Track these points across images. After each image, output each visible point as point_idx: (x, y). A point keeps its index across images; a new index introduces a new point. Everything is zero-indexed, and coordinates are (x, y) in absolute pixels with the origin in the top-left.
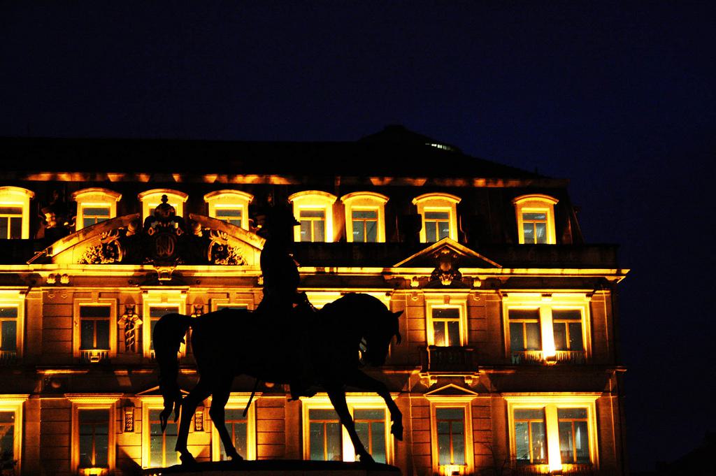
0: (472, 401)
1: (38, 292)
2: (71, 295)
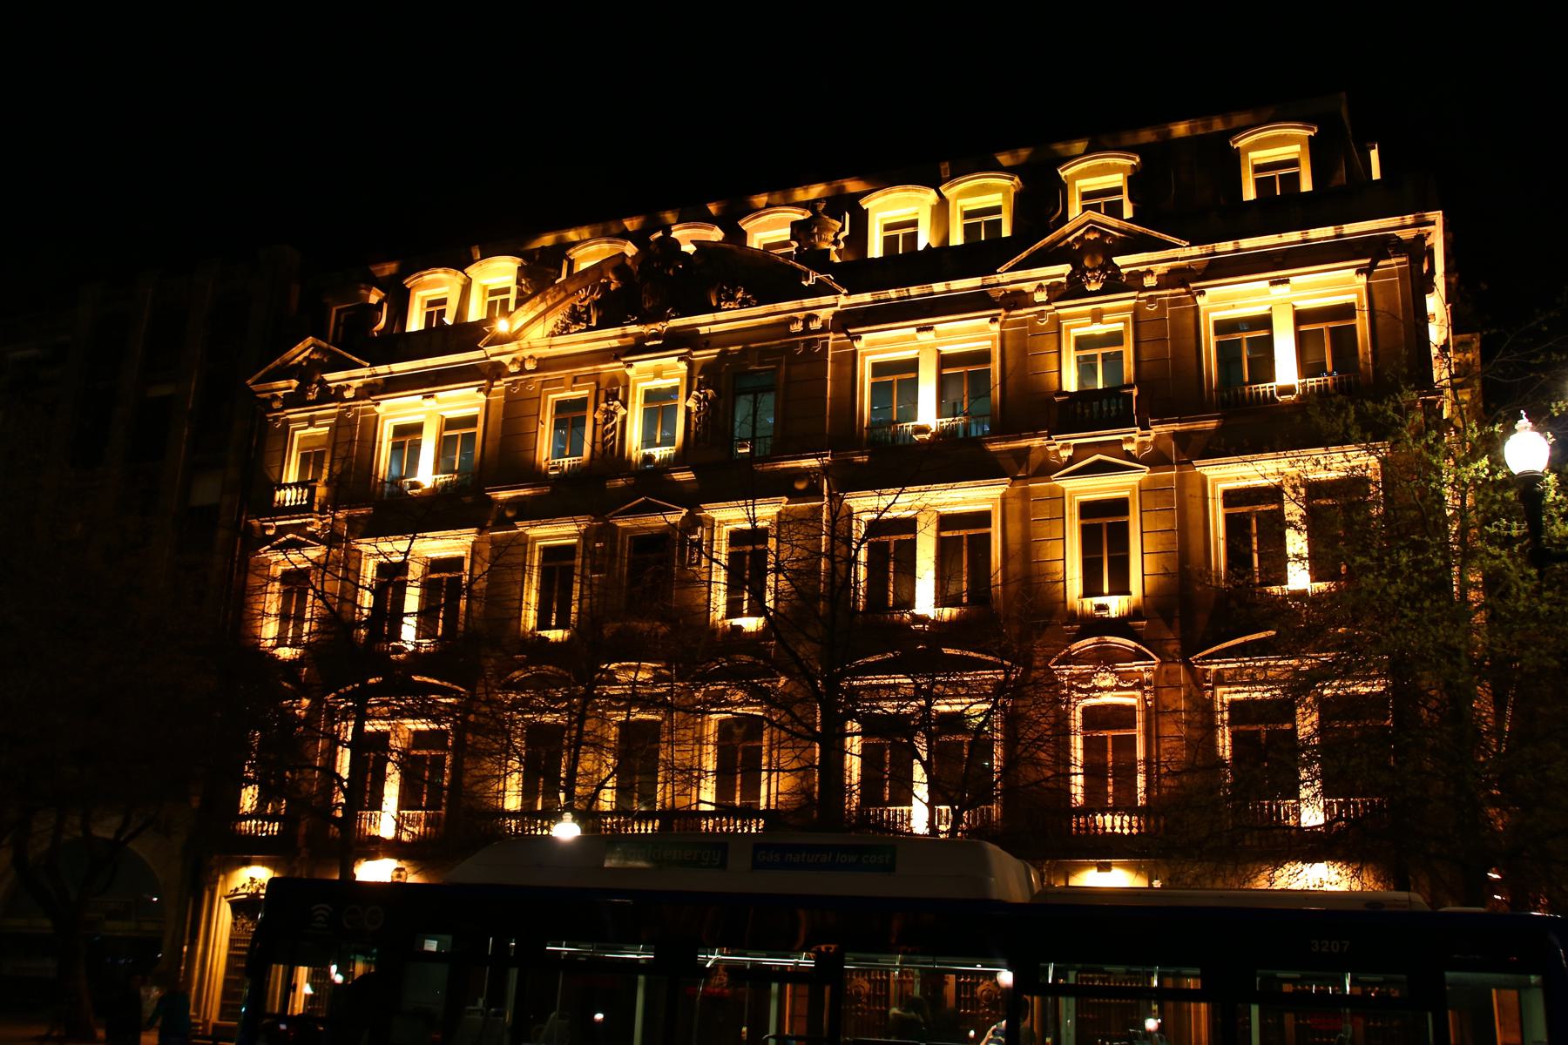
1: (500, 385)
2: (539, 384)
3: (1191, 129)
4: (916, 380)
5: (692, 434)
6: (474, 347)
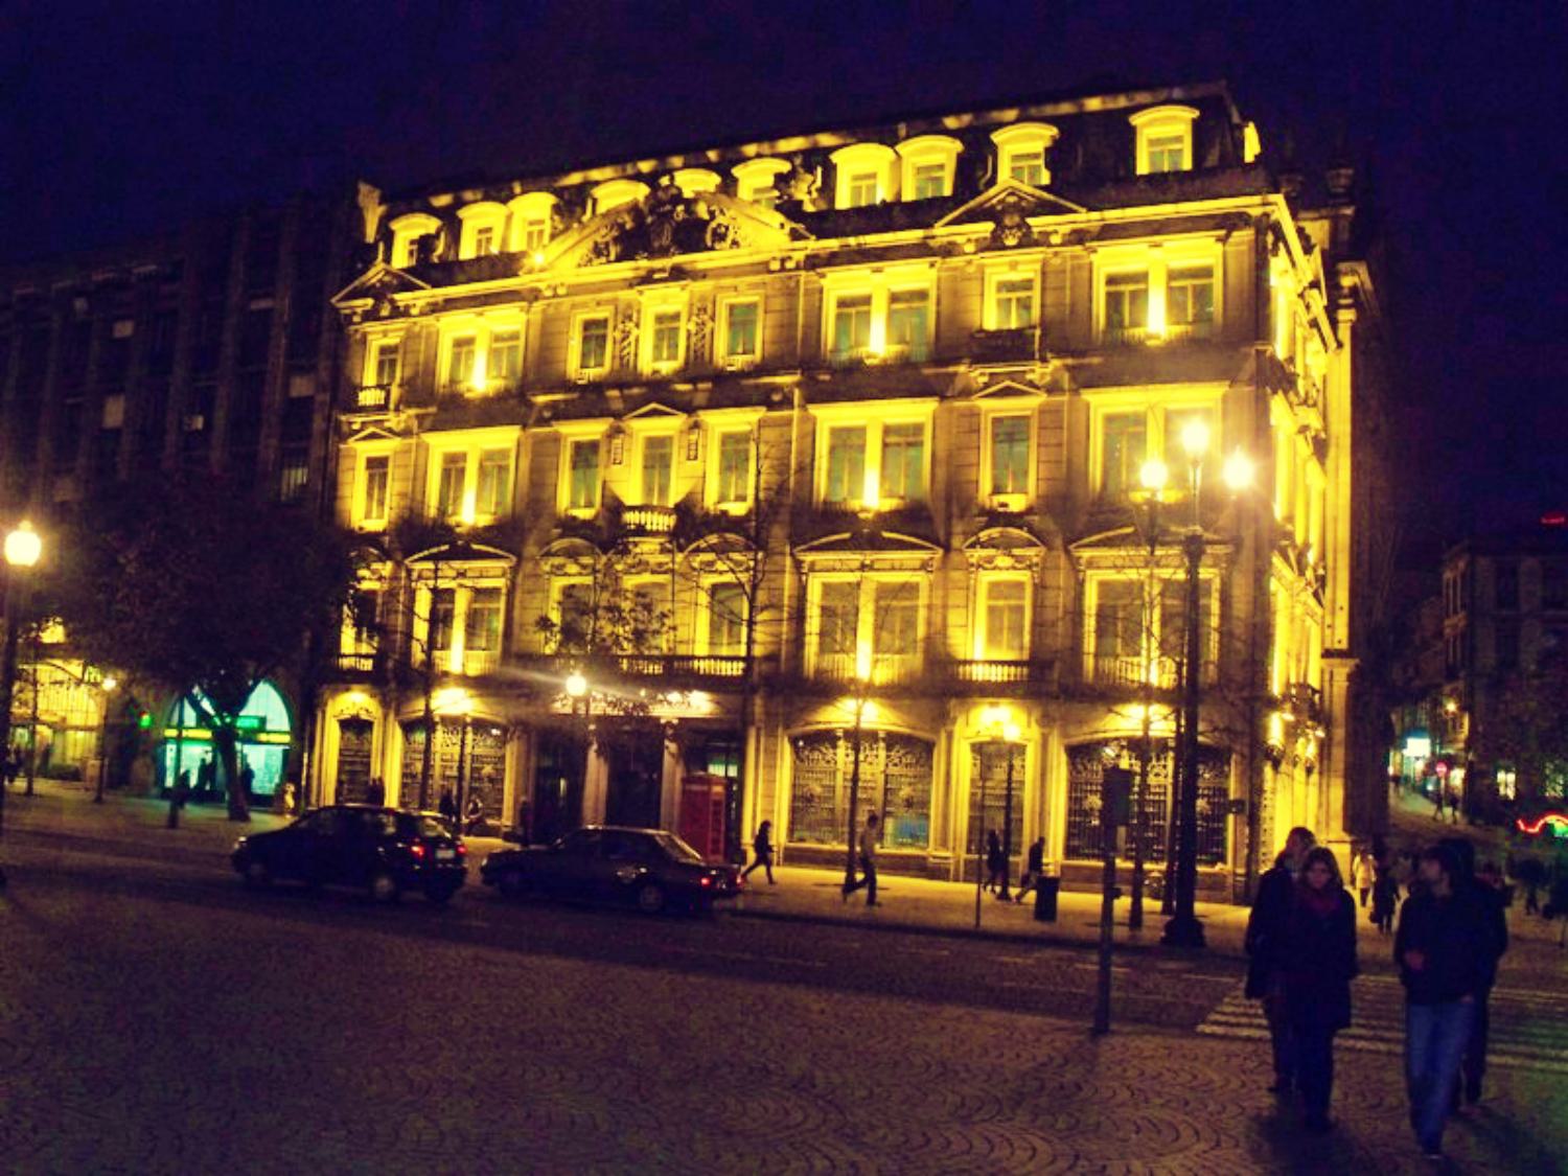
0: (1040, 405)
1: (538, 306)
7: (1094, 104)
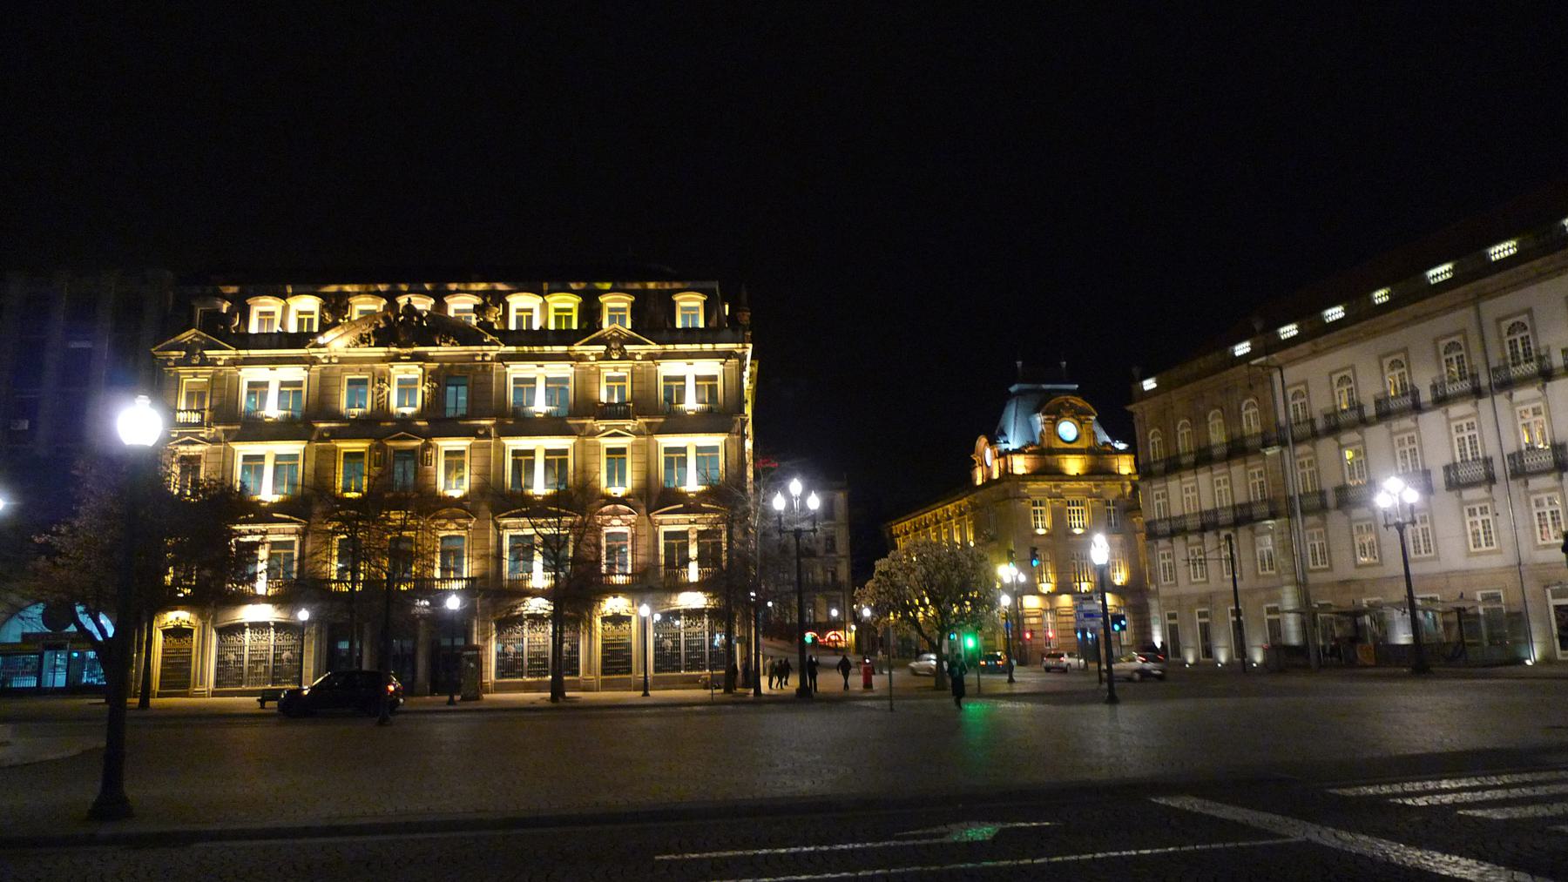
1: (315, 368)
3: (657, 286)
4: (534, 389)
5: (426, 403)
6: (302, 347)
7: (651, 285)
